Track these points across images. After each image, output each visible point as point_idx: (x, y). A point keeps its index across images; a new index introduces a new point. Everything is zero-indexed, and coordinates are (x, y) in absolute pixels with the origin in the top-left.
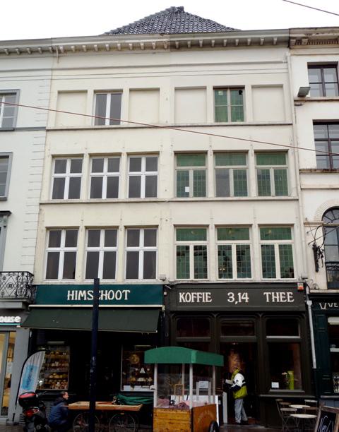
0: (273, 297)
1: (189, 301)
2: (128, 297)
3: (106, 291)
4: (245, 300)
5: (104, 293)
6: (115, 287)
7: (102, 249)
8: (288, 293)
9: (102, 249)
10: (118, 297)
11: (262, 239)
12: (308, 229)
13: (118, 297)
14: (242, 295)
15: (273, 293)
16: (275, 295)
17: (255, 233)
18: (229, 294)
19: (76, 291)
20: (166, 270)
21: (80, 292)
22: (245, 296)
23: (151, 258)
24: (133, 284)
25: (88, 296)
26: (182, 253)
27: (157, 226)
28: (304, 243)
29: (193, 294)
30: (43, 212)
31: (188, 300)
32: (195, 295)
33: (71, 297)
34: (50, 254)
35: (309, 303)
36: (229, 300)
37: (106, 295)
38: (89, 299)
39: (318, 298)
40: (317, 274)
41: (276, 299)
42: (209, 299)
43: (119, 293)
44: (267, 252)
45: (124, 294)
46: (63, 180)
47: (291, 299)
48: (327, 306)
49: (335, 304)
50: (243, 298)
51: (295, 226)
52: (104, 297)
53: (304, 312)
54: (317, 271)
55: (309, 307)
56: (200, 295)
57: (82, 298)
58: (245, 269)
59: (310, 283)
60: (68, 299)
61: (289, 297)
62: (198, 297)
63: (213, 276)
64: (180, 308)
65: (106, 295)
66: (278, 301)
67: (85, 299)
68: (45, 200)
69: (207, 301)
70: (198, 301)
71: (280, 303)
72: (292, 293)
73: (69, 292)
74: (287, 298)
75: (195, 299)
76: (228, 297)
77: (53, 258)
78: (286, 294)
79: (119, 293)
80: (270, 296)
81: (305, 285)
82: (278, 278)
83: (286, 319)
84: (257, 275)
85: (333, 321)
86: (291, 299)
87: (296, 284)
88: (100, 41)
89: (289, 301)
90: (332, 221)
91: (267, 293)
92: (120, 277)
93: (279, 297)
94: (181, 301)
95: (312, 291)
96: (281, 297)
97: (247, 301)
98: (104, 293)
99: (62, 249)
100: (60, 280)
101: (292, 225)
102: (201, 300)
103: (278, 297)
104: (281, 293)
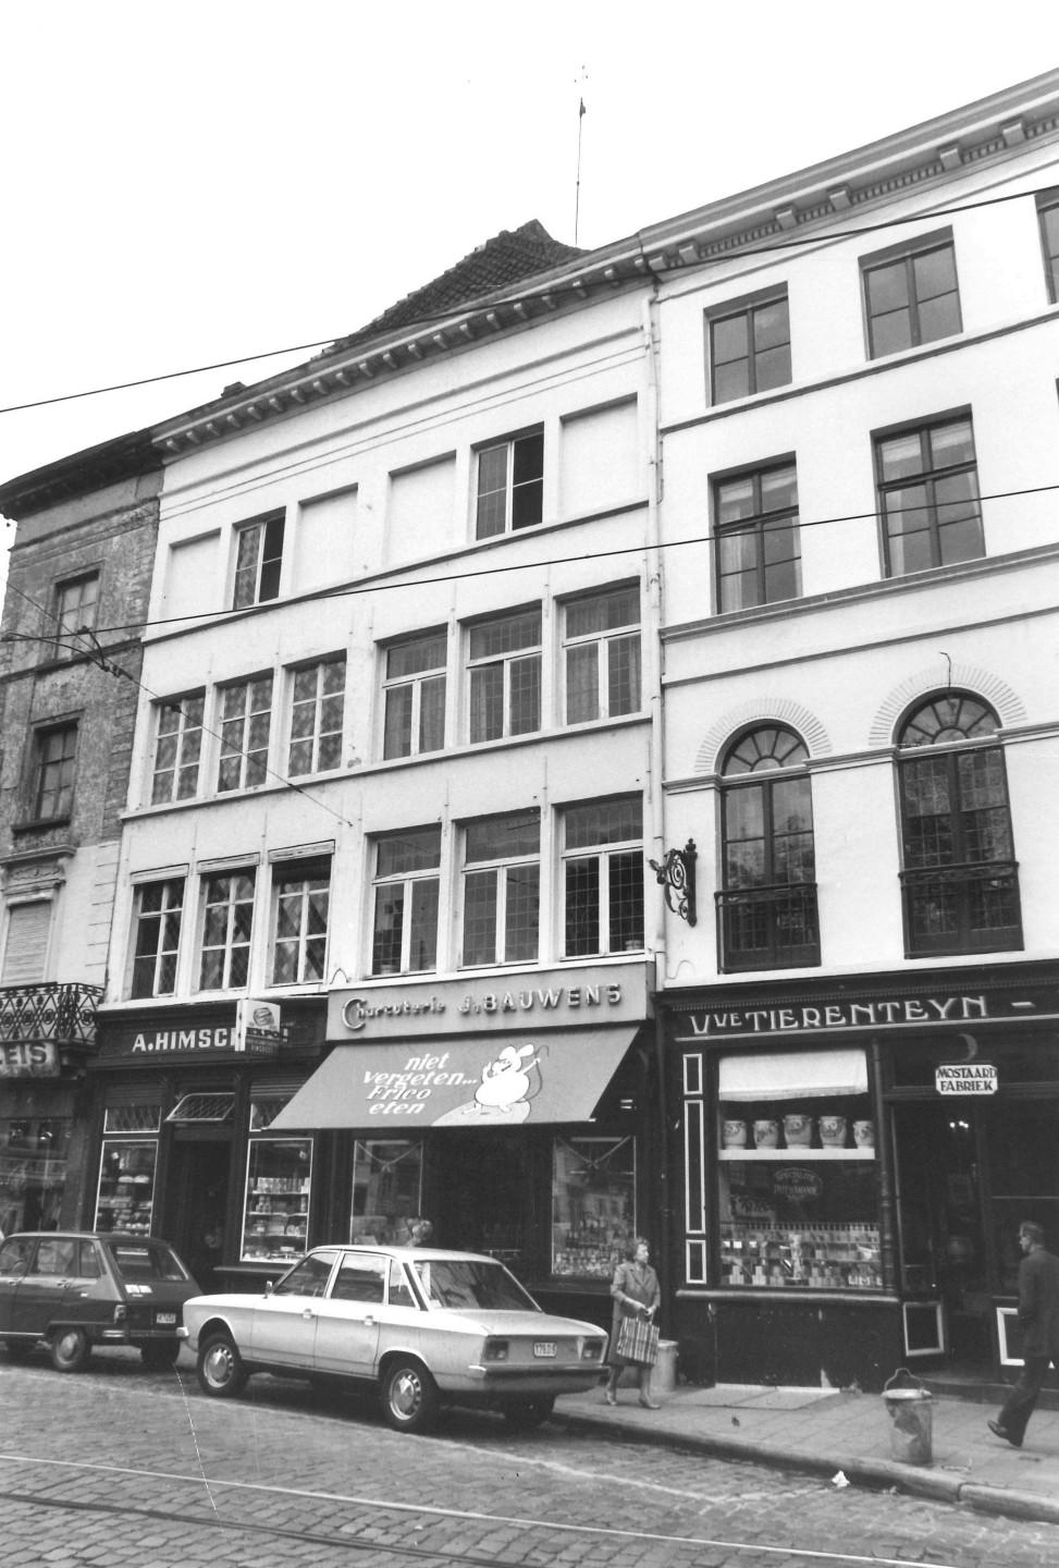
33: (162, 1045)
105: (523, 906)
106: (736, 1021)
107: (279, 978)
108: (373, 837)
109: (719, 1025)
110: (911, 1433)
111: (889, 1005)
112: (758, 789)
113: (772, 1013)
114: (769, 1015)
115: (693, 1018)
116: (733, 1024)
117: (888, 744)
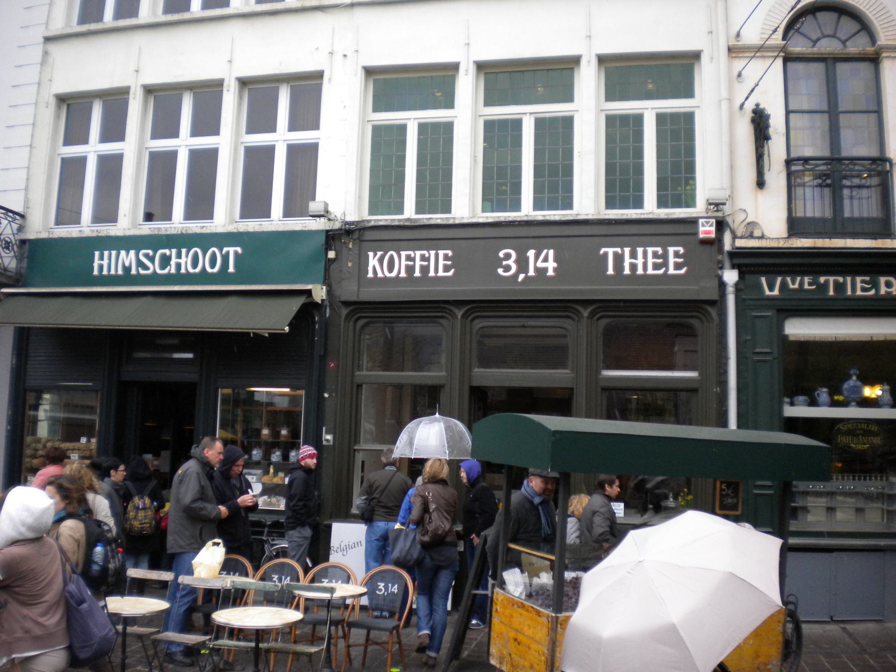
0: (627, 261)
1: (394, 274)
2: (236, 266)
3: (184, 251)
5: (179, 256)
6: (205, 241)
7: (184, 143)
8: (671, 250)
9: (184, 143)
10: (213, 265)
11: (610, 97)
12: (738, 64)
13: (213, 265)
15: (627, 250)
16: (633, 255)
17: (588, 82)
18: (501, 254)
19: (114, 253)
20: (342, 192)
21: (123, 253)
22: (546, 260)
23: (304, 160)
24: (251, 230)
25: (140, 264)
26: (386, 145)
27: (319, 75)
28: (725, 105)
29: (403, 254)
30: (50, 60)
31: (391, 269)
32: (409, 258)
33: (101, 267)
34: (66, 162)
35: (731, 276)
36: (500, 271)
37: (182, 261)
38: (142, 272)
39: (755, 263)
40: (761, 195)
41: (633, 267)
42: (446, 269)
43: (214, 254)
44: (622, 135)
45: (226, 258)
46: (269, 152)
48: (784, 286)
49: (807, 280)
50: (540, 264)
51: (704, 58)
52: (178, 266)
53: (712, 303)
54: (761, 183)
55: (730, 290)
56: (423, 258)
57: (127, 269)
58: (556, 181)
59: (737, 222)
60: (96, 272)
61: (672, 260)
62: (418, 263)
63: (466, 203)
64: (369, 294)
65: (182, 261)
66: (640, 271)
67: (134, 272)
68: (58, 26)
69: (441, 273)
70: (417, 274)
71: (646, 278)
72: (681, 250)
73: (97, 253)
74: (665, 264)
77: (72, 170)
78: (665, 256)
79: (214, 254)
80: (619, 259)
81: (721, 225)
82: (650, 208)
83: (661, 322)
84: (588, 199)
86: (678, 266)
87: (693, 222)
89: (672, 271)
90: (815, 42)
91: (611, 251)
92: (225, 214)
93: (642, 261)
94: (370, 275)
95: (740, 243)
96: (651, 261)
97: (551, 273)
98: (179, 256)
99: (93, 149)
100: (87, 226)
101: (696, 56)
102: (425, 270)
103: (640, 261)
104: (650, 250)
105: (501, 172)
106: (810, 284)
107: (246, 213)
108: (369, 72)
109: (791, 286)
110: (494, 495)
111: (831, 279)
112: (819, 67)
113: (849, 279)
114: (138, 270)
115: (763, 280)
116: (806, 287)
117: (777, 39)
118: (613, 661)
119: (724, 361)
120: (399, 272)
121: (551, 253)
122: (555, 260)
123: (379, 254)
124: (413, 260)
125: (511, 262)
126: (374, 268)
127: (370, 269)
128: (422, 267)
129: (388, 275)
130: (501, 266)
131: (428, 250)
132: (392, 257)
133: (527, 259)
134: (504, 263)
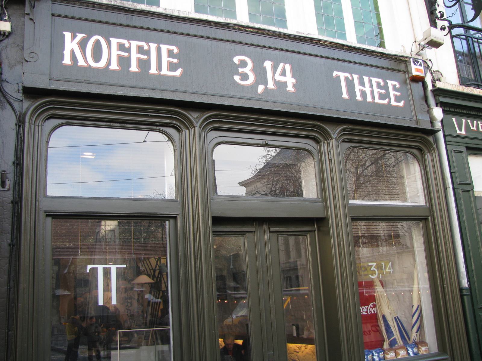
0: (358, 88)
1: (102, 64)
4: (285, 84)
14: (275, 69)
22: (283, 74)
29: (114, 41)
36: (237, 78)
41: (363, 94)
47: (397, 99)
56: (140, 50)
61: (392, 93)
62: (135, 56)
70: (134, 68)
72: (175, 50)
75: (124, 62)
76: (234, 69)
78: (386, 87)
80: (350, 84)
85: (5, 26)
88: (458, 302)
89: (393, 103)
94: (67, 60)
97: (290, 88)
102: (144, 64)
103: (367, 89)
105: (210, 23)
118: (285, 352)
119: (404, 191)
120: (109, 63)
121: (288, 67)
122: (294, 76)
123: (80, 36)
124: (128, 50)
125: (248, 70)
126: (73, 52)
127: (67, 54)
128: (139, 60)
129: (93, 64)
130: (237, 73)
131: (147, 42)
132: (98, 43)
133: (265, 69)
134: (240, 70)
